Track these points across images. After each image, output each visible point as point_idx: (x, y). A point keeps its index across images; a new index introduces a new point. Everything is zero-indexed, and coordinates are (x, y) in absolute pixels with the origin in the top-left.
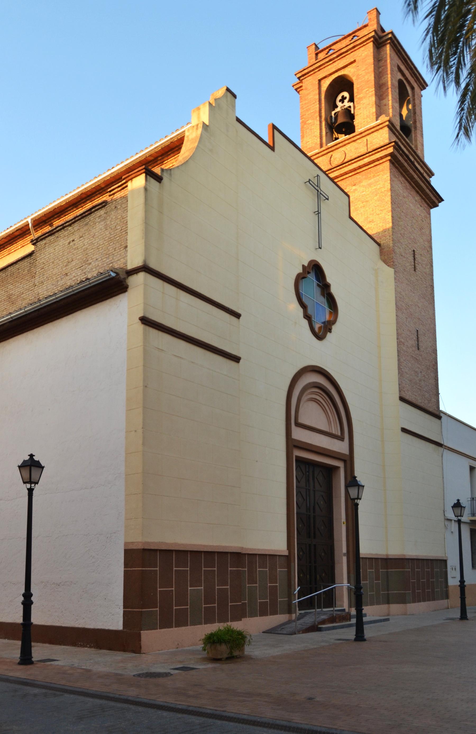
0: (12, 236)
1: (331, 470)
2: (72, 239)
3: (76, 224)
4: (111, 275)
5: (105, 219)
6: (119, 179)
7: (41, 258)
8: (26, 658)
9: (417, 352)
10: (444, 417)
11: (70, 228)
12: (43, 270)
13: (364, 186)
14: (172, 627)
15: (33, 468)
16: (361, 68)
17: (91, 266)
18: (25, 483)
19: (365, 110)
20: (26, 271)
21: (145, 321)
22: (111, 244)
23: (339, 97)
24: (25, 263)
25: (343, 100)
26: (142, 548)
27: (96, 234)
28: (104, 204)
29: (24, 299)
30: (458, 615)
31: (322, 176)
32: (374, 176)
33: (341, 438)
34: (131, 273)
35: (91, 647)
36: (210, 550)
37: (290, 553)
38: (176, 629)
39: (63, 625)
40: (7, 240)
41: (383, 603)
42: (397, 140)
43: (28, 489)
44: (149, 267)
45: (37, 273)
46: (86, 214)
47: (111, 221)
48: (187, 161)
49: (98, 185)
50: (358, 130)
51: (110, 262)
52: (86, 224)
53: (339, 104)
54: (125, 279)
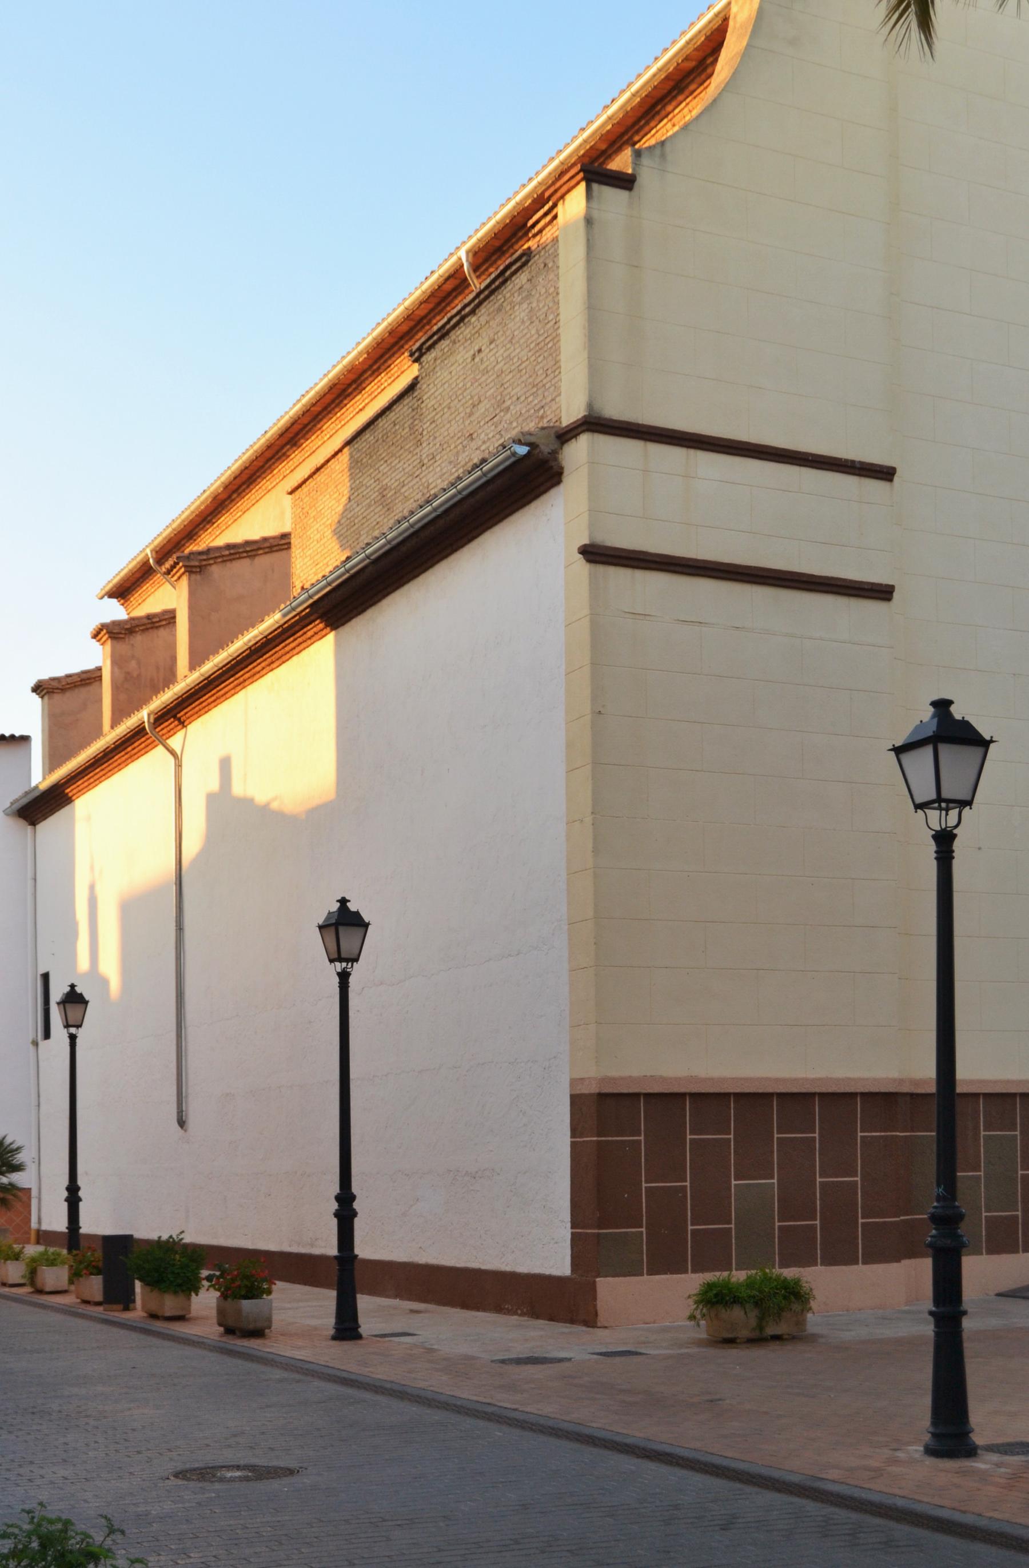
0: (441, 295)
2: (477, 348)
3: (483, 310)
4: (514, 454)
5: (529, 295)
6: (544, 201)
7: (430, 394)
8: (347, 1327)
11: (474, 319)
12: (434, 425)
14: (686, 1272)
15: (341, 929)
17: (509, 415)
18: (331, 961)
20: (407, 430)
21: (595, 554)
22: (540, 360)
24: (403, 410)
26: (597, 1091)
27: (516, 333)
28: (524, 259)
34: (566, 435)
35: (523, 1314)
36: (795, 1090)
38: (693, 1276)
39: (483, 1267)
40: (431, 306)
43: (339, 974)
44: (599, 418)
45: (425, 433)
46: (497, 283)
47: (538, 301)
48: (715, 100)
49: (591, 147)
51: (539, 406)
52: (499, 310)
54: (554, 454)
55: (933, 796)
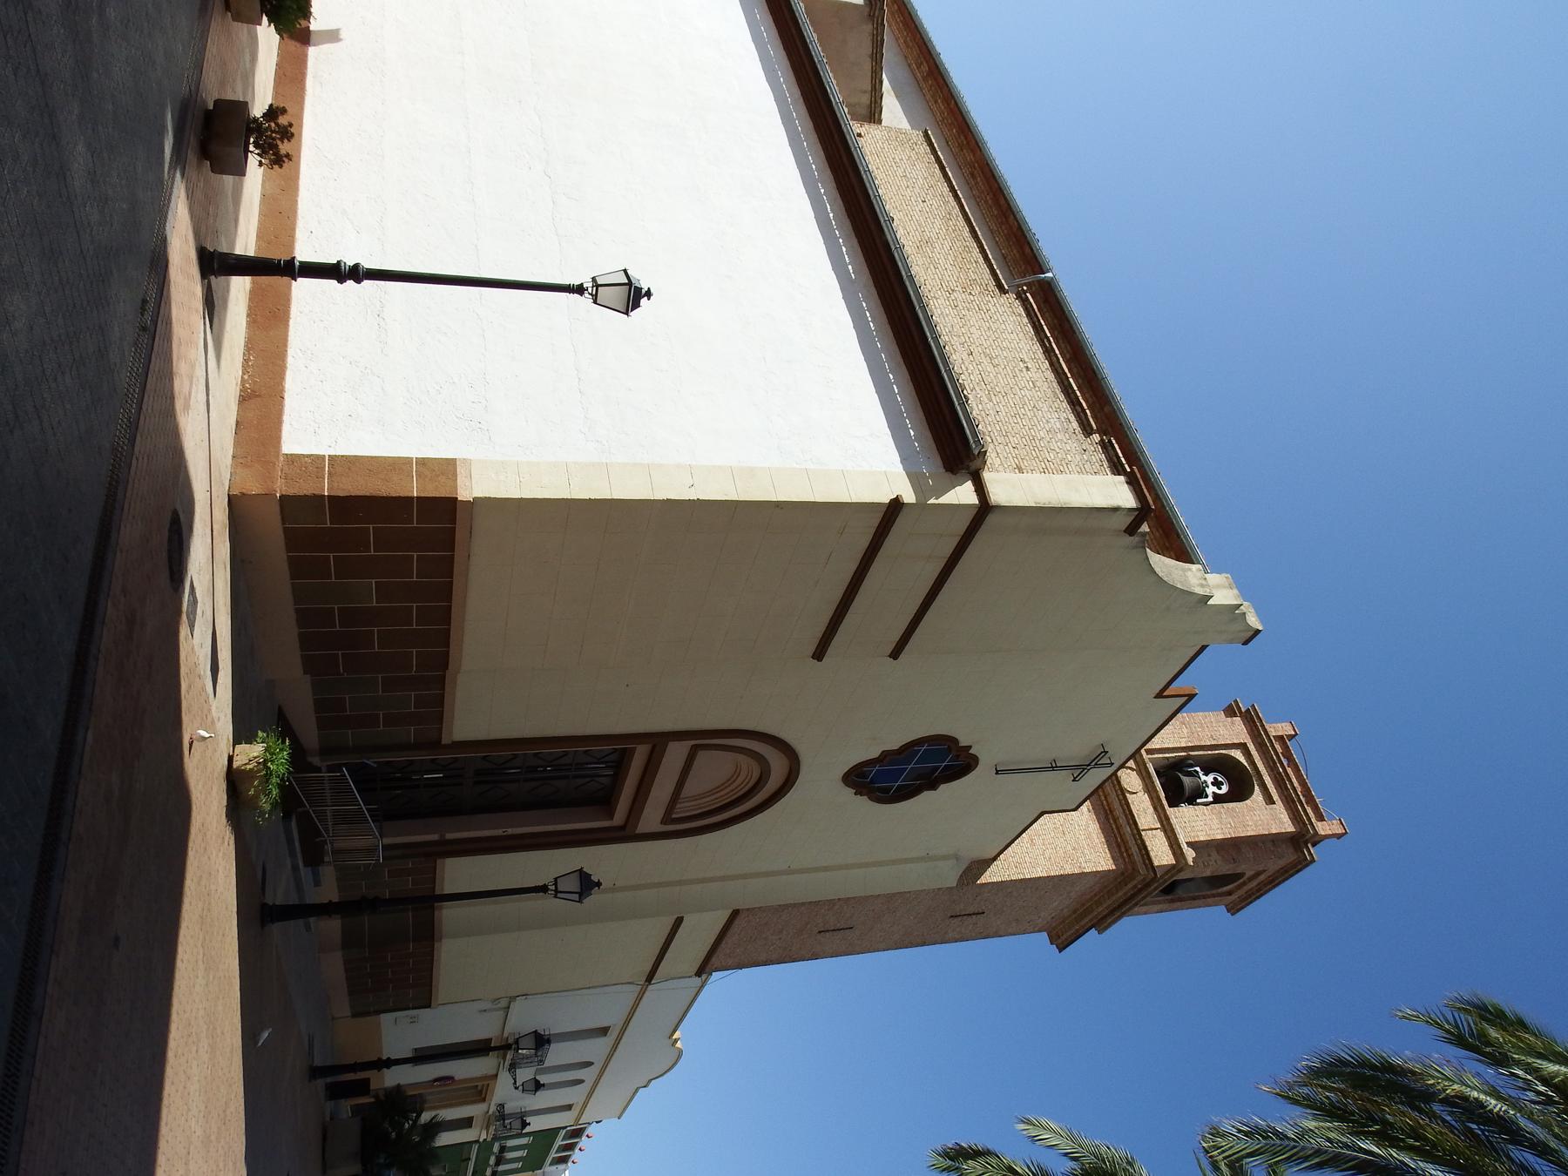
1: (605, 802)
9: (816, 930)
10: (698, 981)
16: (1261, 816)
18: (594, 279)
19: (1201, 823)
25: (1216, 783)
30: (318, 1062)
31: (1110, 771)
37: (446, 746)
50: (1170, 811)
53: (1210, 779)
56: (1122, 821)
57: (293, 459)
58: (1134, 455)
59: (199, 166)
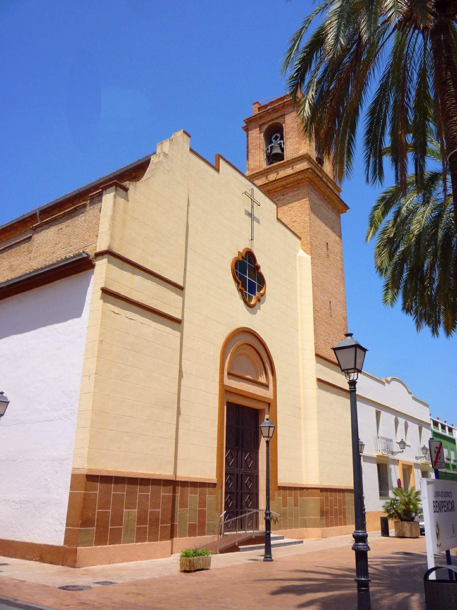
13: (290, 196)
23: (274, 137)
26: (86, 473)
29: (21, 269)
32: (297, 190)
33: (266, 386)
41: (163, 538)
42: (313, 167)
50: (285, 160)
55: (353, 367)
56: (288, 181)
57: (66, 542)
58: (95, 187)
59: (435, 184)
